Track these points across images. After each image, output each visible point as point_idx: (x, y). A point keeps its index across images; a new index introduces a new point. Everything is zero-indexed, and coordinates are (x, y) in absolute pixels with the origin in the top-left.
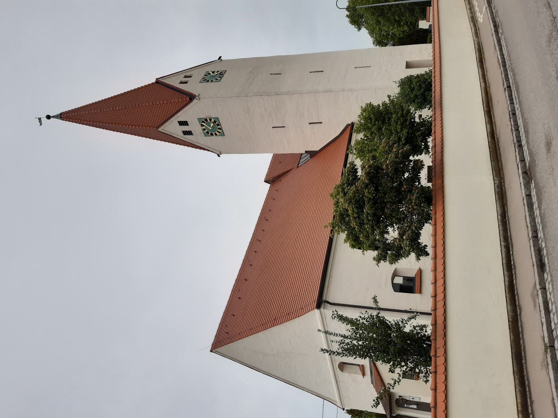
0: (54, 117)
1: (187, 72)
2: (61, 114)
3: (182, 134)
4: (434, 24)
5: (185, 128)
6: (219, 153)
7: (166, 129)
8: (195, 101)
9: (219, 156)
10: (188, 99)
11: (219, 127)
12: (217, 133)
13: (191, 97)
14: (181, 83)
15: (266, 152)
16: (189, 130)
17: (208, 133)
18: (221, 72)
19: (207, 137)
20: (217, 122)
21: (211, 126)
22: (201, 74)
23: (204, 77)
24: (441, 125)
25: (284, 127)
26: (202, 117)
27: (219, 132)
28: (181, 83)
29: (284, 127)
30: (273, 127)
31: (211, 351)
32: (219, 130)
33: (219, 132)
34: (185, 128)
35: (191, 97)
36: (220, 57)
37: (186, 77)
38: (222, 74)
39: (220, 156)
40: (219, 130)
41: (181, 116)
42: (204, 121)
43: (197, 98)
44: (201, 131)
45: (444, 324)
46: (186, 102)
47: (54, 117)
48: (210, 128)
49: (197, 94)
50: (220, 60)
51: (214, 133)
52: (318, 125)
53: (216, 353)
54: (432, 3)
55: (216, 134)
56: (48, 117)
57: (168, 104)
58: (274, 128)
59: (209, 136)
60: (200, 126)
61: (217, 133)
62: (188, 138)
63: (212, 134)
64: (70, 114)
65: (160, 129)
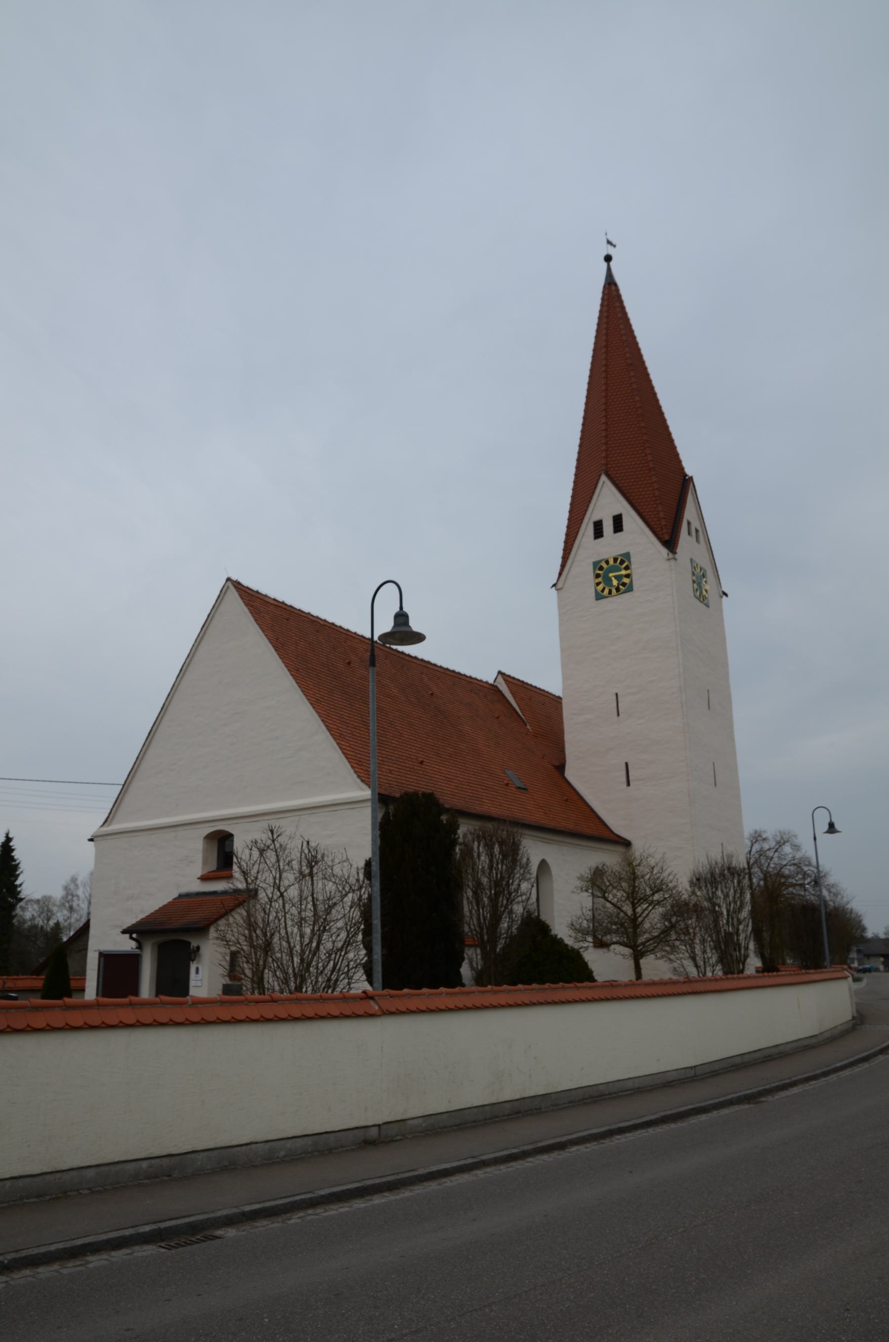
0: (609, 269)
1: (703, 533)
2: (616, 285)
3: (596, 518)
4: (745, 978)
5: (608, 527)
6: (559, 586)
7: (605, 489)
8: (664, 551)
9: (554, 585)
10: (667, 537)
11: (614, 591)
12: (600, 587)
13: (670, 543)
14: (689, 523)
15: (565, 678)
16: (605, 533)
17: (601, 568)
18: (706, 598)
19: (591, 567)
20: (625, 587)
21: (613, 579)
22: (705, 563)
23: (699, 566)
24: (520, 1002)
25: (618, 715)
26: (632, 560)
27: (603, 591)
28: (689, 523)
29: (618, 715)
30: (617, 694)
31: (228, 579)
32: (606, 591)
33: (603, 591)
34: (608, 527)
35: (670, 543)
36: (726, 595)
37: (697, 531)
38: (704, 600)
39: (554, 588)
40: (606, 591)
41: (632, 521)
42: (624, 560)
43: (671, 555)
44: (605, 557)
45: (4, 1029)
46: (661, 533)
47: (609, 269)
48: (611, 575)
49: (677, 556)
50: (721, 594)
51: (600, 580)
52: (624, 779)
53: (223, 592)
54: (775, 973)
55: (598, 584)
56: (608, 259)
57: (654, 499)
58: (615, 697)
59: (594, 571)
60: (615, 554)
61: (600, 587)
62: (587, 529)
63: (598, 576)
64: (618, 304)
65: (604, 478)
